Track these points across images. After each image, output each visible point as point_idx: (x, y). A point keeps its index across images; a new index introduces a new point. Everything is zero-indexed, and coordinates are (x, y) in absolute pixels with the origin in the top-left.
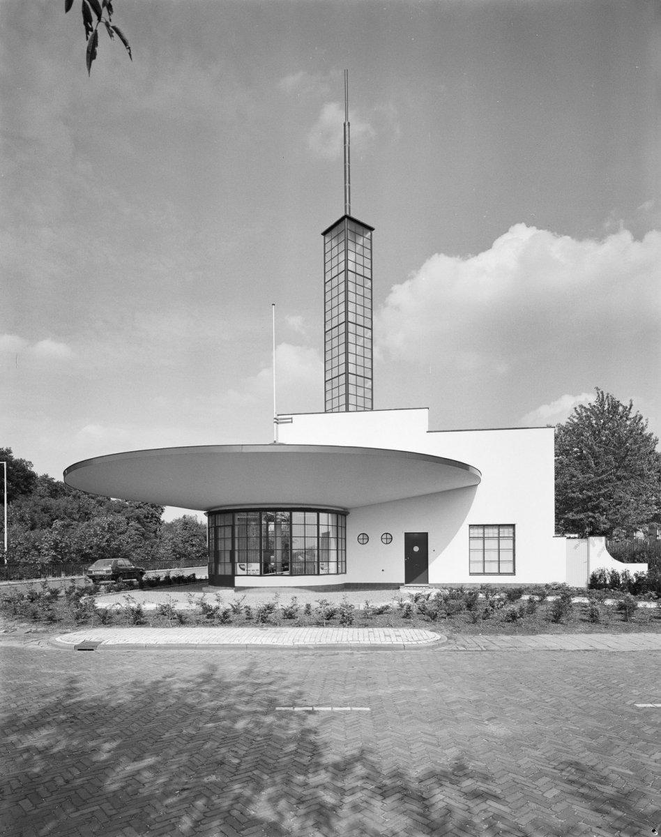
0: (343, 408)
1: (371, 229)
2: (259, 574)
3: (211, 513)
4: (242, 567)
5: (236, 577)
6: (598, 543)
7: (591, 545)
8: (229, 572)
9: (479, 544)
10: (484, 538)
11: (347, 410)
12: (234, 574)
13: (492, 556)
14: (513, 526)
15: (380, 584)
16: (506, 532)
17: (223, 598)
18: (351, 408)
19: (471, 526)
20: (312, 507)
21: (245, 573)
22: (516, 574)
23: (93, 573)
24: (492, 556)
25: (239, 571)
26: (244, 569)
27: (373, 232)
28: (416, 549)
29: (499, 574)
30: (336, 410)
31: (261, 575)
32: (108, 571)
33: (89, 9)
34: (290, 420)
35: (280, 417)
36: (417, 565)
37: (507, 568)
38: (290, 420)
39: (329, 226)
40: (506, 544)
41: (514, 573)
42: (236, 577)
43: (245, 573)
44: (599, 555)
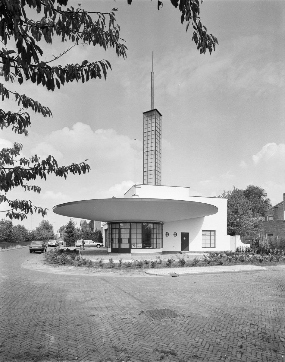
0: (154, 183)
1: (161, 115)
2: (141, 248)
3: (110, 223)
4: (134, 245)
5: (131, 249)
6: (238, 237)
7: (237, 238)
8: (127, 246)
9: (205, 236)
10: (206, 235)
11: (155, 185)
12: (130, 247)
13: (208, 241)
14: (215, 231)
15: (173, 252)
16: (213, 233)
17: (126, 259)
18: (157, 184)
19: (203, 231)
20: (117, 222)
21: (135, 247)
22: (216, 247)
23: (33, 248)
24: (208, 241)
25: (133, 247)
26: (135, 246)
27: (162, 117)
28: (185, 238)
29: (210, 248)
30: (150, 184)
31: (142, 248)
32: (40, 247)
33: (51, 11)
34: (140, 187)
35: (136, 185)
36: (185, 245)
37: (213, 245)
38: (140, 187)
39: (161, 113)
40: (213, 237)
41: (215, 247)
42: (131, 249)
43: (135, 247)
44: (238, 241)
